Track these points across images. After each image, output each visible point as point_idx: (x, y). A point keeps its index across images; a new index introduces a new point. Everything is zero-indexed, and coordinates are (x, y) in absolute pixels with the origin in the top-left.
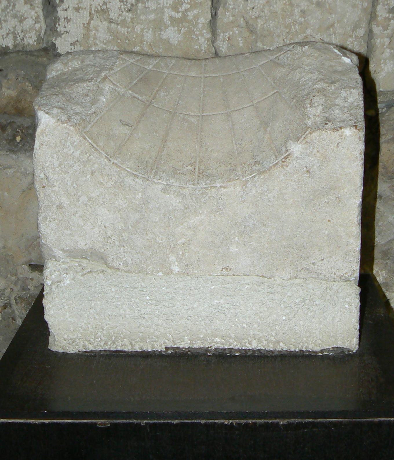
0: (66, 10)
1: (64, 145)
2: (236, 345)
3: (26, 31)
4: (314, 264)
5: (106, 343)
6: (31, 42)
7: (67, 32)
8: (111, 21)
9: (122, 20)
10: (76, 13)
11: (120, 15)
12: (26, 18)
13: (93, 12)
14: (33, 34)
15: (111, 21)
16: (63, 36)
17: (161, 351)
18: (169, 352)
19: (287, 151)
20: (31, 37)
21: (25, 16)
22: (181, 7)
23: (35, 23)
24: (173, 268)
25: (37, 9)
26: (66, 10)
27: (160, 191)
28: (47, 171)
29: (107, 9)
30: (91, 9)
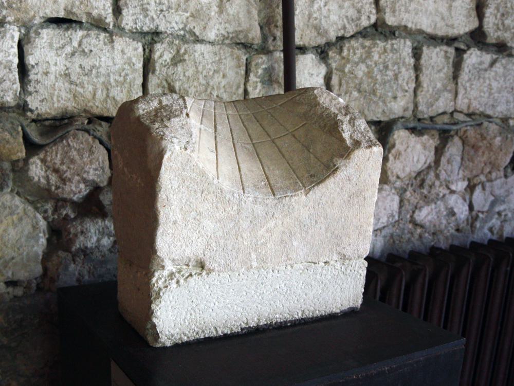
0: (37, 74)
1: (184, 169)
2: (289, 318)
3: (5, 90)
4: (344, 248)
5: (197, 333)
6: (9, 99)
7: (36, 92)
8: (71, 83)
9: (80, 83)
10: (44, 77)
11: (78, 78)
12: (5, 80)
13: (58, 76)
14: (10, 93)
15: (71, 83)
16: (33, 95)
17: (238, 332)
18: (244, 331)
19: (335, 165)
20: (9, 96)
21: (4, 78)
22: (333, 52)
23: (13, 84)
24: (252, 264)
25: (14, 73)
26: (37, 74)
27: (429, 185)
28: (168, 192)
29: (69, 73)
30: (56, 73)
